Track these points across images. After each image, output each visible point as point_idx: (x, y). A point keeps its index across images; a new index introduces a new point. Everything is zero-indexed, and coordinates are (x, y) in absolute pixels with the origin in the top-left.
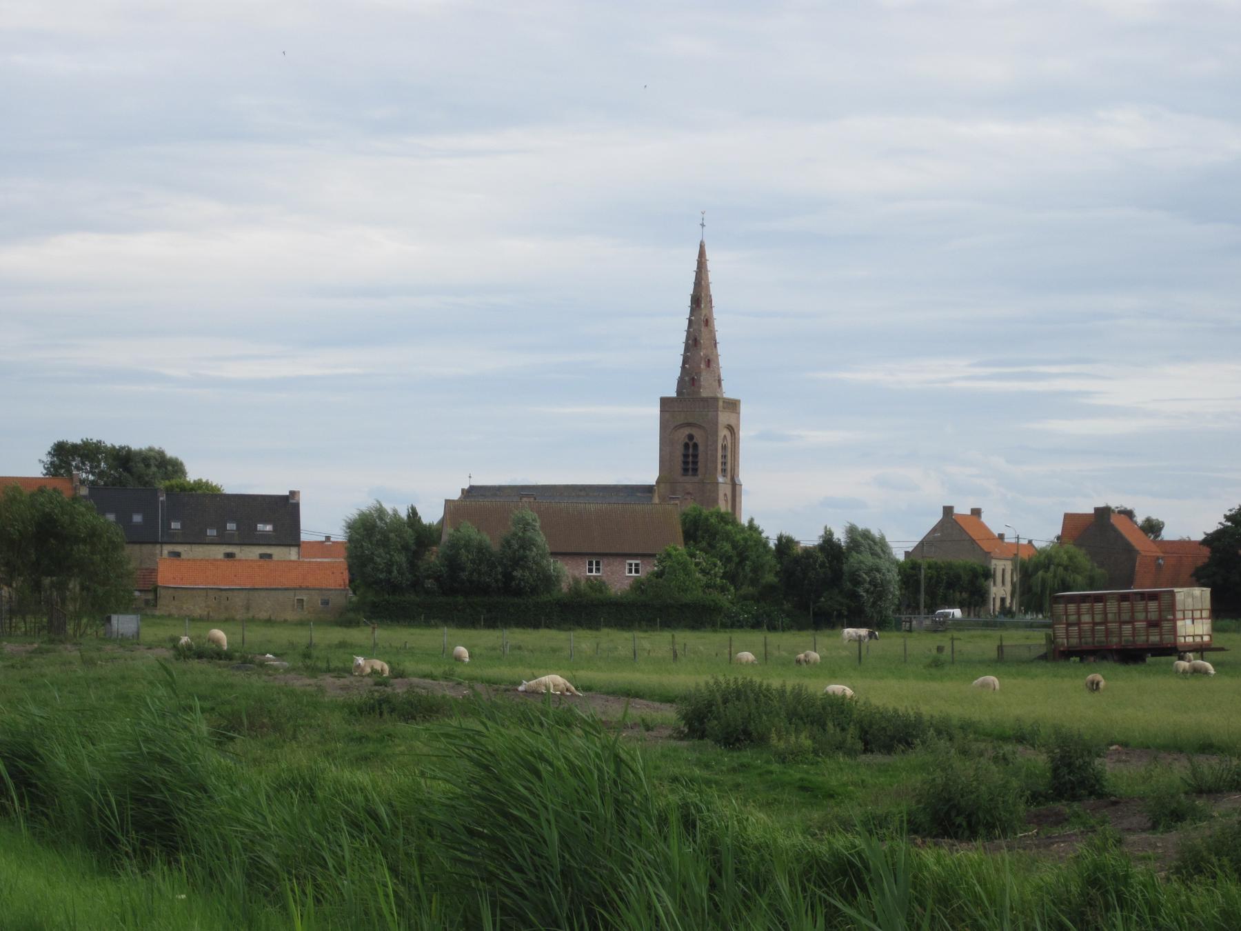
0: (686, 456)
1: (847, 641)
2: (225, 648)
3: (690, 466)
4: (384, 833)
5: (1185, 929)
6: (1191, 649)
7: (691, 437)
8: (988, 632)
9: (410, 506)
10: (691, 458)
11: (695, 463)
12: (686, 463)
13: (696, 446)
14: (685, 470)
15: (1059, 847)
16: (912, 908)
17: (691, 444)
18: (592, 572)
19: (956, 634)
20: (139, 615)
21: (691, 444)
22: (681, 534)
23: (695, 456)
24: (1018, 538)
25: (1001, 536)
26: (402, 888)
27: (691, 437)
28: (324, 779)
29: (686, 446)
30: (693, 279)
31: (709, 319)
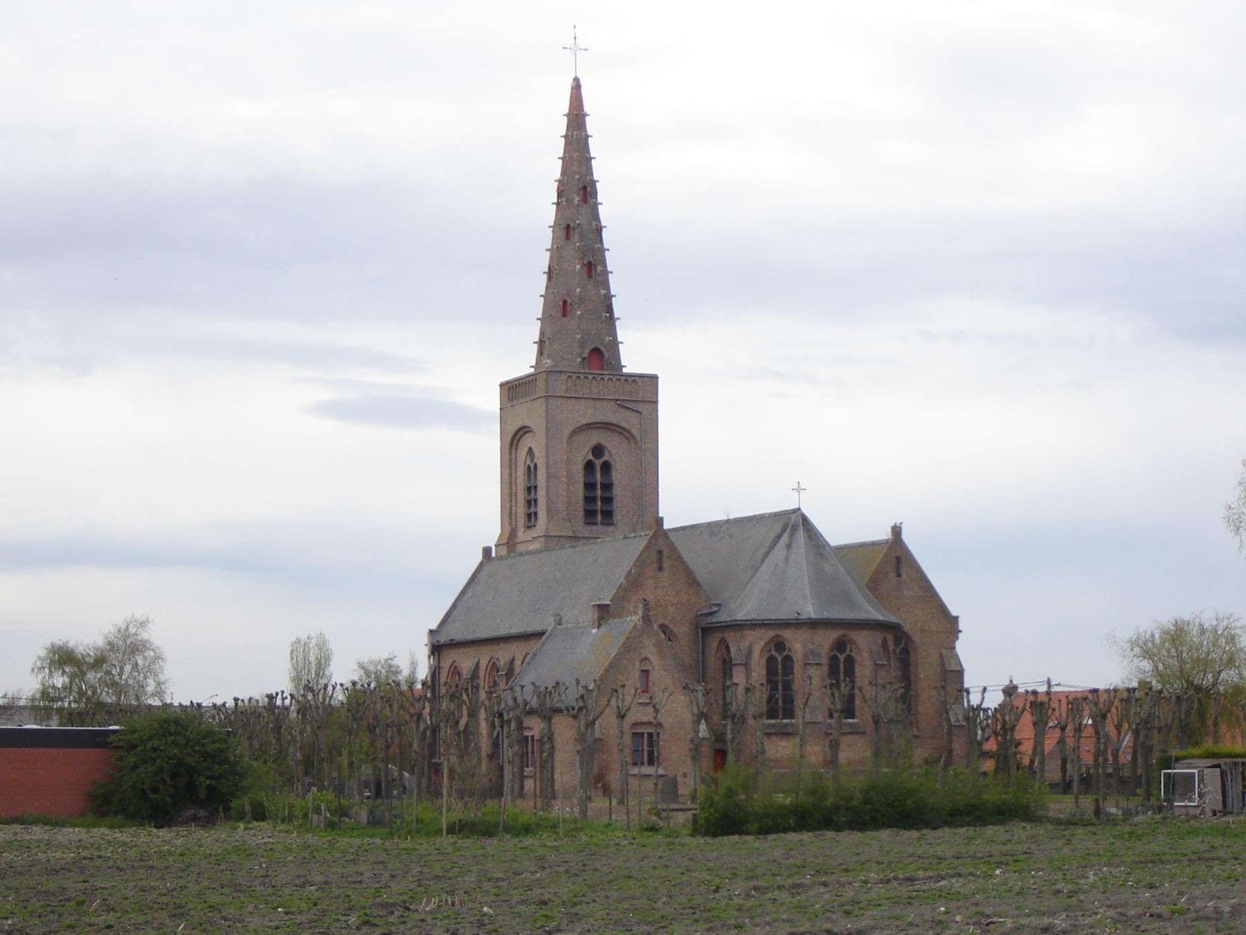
0: (589, 486)
1: (394, 679)
4: (160, 894)
7: (598, 450)
9: (356, 667)
10: (599, 503)
11: (608, 500)
12: (589, 499)
13: (606, 467)
14: (590, 515)
15: (923, 862)
17: (598, 463)
18: (649, 733)
19: (653, 720)
21: (598, 463)
23: (607, 487)
24: (1049, 682)
25: (224, 705)
27: (598, 450)
29: (589, 466)
31: (527, 520)
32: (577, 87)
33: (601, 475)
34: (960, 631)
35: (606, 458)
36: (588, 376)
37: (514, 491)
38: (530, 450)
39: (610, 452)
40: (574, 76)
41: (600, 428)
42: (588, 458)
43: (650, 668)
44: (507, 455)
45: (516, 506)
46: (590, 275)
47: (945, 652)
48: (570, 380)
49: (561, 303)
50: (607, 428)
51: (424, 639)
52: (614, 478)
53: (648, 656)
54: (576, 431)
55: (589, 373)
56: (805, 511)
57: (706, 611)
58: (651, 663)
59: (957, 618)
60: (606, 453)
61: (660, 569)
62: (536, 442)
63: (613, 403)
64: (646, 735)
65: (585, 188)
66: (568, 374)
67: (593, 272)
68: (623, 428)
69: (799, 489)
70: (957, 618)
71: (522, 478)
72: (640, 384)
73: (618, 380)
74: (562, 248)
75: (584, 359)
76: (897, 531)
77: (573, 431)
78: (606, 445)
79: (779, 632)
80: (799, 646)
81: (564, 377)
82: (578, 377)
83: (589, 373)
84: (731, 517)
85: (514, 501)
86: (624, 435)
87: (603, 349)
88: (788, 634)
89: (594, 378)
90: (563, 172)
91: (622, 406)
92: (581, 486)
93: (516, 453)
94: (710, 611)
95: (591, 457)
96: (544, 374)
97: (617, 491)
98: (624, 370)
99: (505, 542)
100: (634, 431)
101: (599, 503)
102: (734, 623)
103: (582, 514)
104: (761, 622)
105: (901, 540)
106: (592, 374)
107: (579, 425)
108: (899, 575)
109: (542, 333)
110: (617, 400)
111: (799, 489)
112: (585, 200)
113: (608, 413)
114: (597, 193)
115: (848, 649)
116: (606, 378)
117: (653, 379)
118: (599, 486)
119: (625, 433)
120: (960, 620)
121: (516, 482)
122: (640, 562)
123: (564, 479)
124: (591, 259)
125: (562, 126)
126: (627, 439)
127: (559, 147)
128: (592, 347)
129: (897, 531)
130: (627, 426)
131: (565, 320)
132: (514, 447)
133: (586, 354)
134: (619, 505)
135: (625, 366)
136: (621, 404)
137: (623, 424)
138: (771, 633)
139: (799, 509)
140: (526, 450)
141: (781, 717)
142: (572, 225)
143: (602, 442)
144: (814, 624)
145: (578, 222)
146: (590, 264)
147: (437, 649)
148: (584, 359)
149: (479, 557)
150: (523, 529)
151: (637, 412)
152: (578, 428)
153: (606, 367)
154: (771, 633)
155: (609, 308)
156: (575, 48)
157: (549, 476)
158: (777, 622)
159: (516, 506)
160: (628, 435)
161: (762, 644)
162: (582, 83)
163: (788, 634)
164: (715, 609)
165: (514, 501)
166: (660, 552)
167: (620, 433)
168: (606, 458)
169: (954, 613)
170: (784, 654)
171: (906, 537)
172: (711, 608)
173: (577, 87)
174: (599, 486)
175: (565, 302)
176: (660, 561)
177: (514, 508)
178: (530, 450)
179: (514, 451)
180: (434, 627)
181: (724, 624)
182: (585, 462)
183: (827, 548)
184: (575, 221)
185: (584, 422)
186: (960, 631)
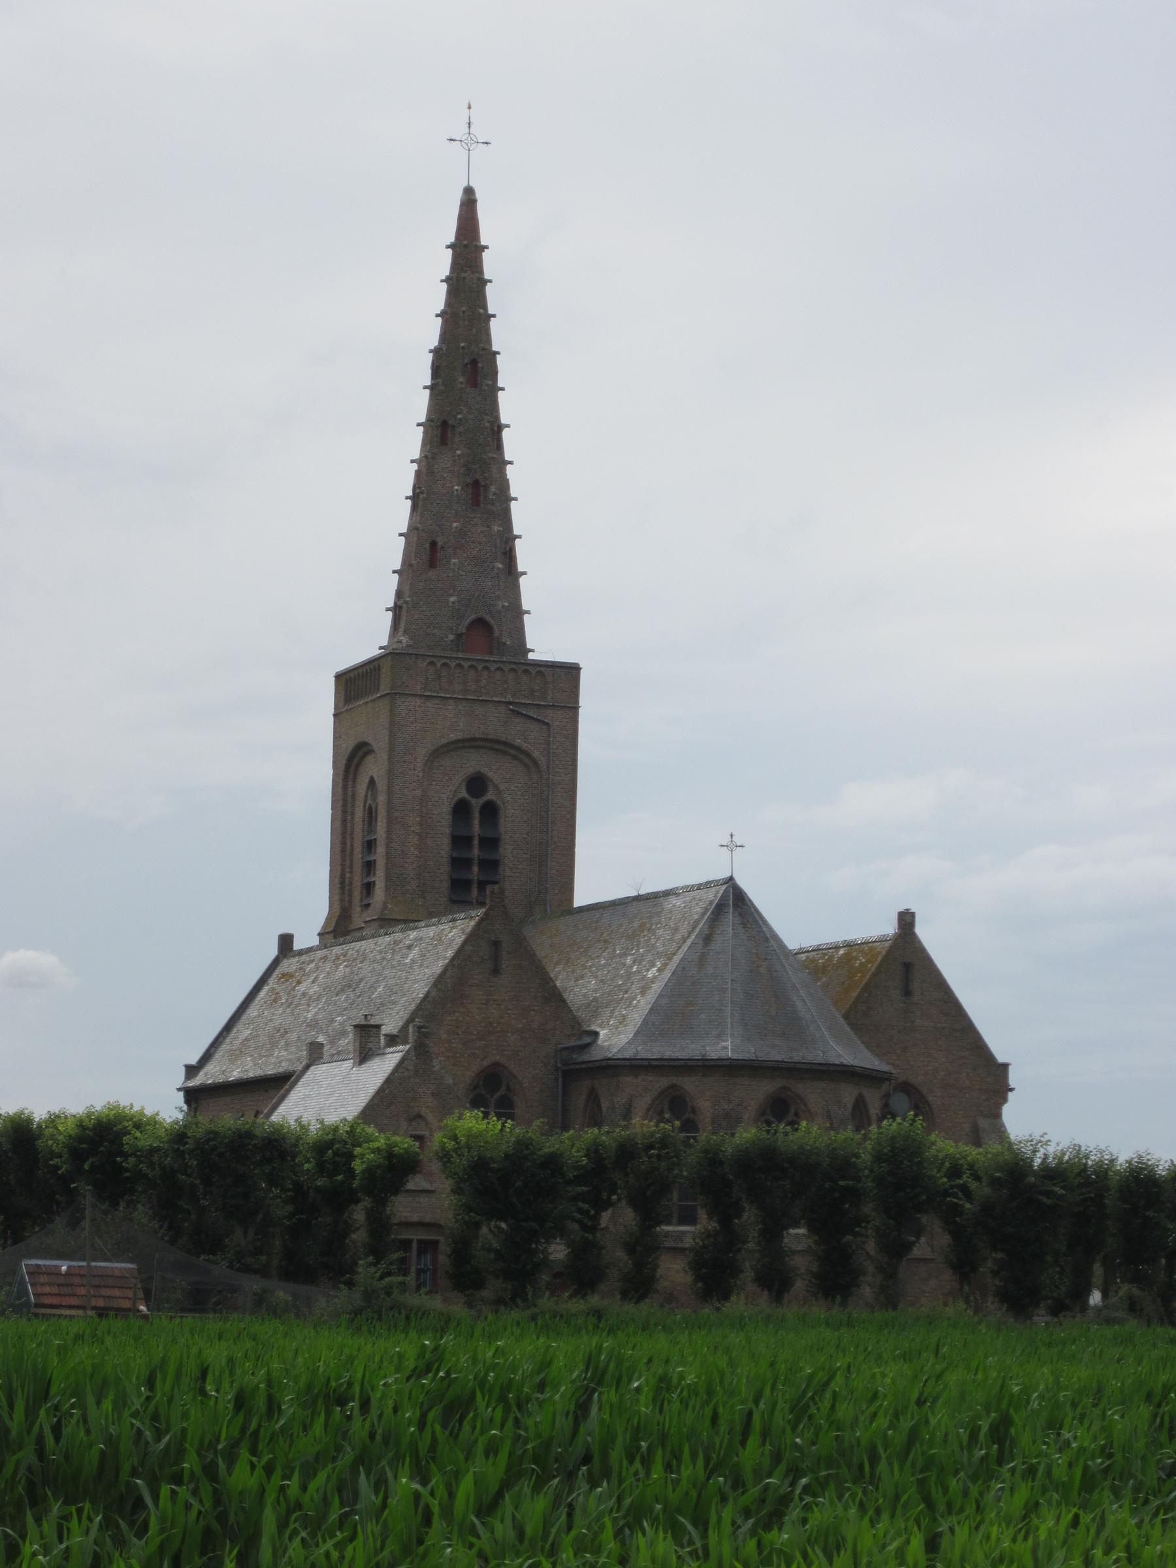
0: (460, 841)
2: (839, 1297)
3: (476, 852)
5: (846, 1550)
6: (220, 1040)
7: (477, 783)
8: (235, 1030)
10: (475, 869)
12: (460, 863)
13: (491, 811)
16: (423, 1030)
17: (476, 804)
20: (352, 1166)
21: (476, 804)
22: (377, 868)
23: (491, 843)
26: (345, 1386)
27: (477, 783)
28: (995, 1143)
29: (461, 810)
30: (431, 333)
31: (364, 892)
32: (469, 203)
33: (481, 823)
34: (1012, 1090)
35: (490, 796)
36: (463, 663)
37: (348, 847)
38: (372, 782)
39: (496, 787)
40: (465, 184)
41: (484, 747)
42: (460, 796)
43: (426, 1133)
44: (340, 789)
45: (351, 872)
46: (476, 501)
47: (983, 1123)
48: (432, 669)
49: (427, 546)
50: (470, 747)
51: (179, 1078)
52: (502, 829)
53: (422, 1113)
54: (438, 753)
55: (463, 659)
56: (742, 882)
57: (572, 1043)
58: (427, 1123)
59: (1005, 1067)
60: (491, 788)
61: (496, 971)
62: (375, 768)
63: (502, 708)
64: (415, 1245)
65: (474, 362)
66: (428, 660)
67: (481, 498)
68: (518, 749)
69: (732, 846)
70: (1005, 1067)
71: (360, 827)
72: (550, 679)
73: (512, 670)
74: (433, 458)
75: (459, 636)
76: (906, 920)
77: (436, 750)
78: (490, 774)
79: (675, 1080)
80: (707, 1104)
81: (423, 664)
82: (445, 665)
83: (450, 658)
84: (642, 893)
85: (348, 863)
86: (521, 761)
87: (492, 622)
88: (689, 1084)
89: (471, 666)
90: (445, 336)
91: (519, 713)
92: (446, 842)
93: (354, 786)
94: (579, 1043)
95: (464, 794)
96: (389, 658)
97: (507, 851)
98: (531, 656)
99: (331, 929)
100: (536, 754)
101: (475, 869)
102: (604, 1063)
103: (446, 884)
104: (646, 1063)
105: (914, 935)
106: (457, 658)
107: (444, 741)
108: (907, 993)
109: (399, 594)
110: (510, 703)
111: (732, 846)
112: (474, 382)
113: (493, 723)
114: (496, 373)
115: (792, 1111)
116: (493, 667)
117: (571, 672)
118: (476, 842)
119: (522, 757)
120: (1010, 1068)
121: (352, 834)
122: (461, 959)
123: (416, 828)
124: (478, 476)
125: (444, 262)
126: (526, 765)
127: (438, 297)
128: (473, 617)
129: (906, 920)
130: (525, 746)
131: (432, 574)
132: (351, 776)
133: (462, 629)
134: (508, 873)
135: (532, 651)
136: (516, 711)
137: (518, 742)
138: (664, 1082)
139: (731, 879)
140: (367, 780)
141: (675, 1221)
142: (451, 422)
143: (485, 770)
144: (731, 1069)
145: (459, 416)
146: (476, 484)
147: (193, 1096)
148: (459, 636)
149: (273, 952)
150: (359, 909)
151: (543, 722)
152: (444, 746)
153: (495, 651)
154: (664, 1082)
155: (509, 556)
156: (469, 141)
157: (390, 820)
158: (672, 1063)
159: (351, 872)
160: (526, 760)
161: (649, 1098)
162: (479, 195)
163: (689, 1084)
164: (587, 1040)
165: (348, 863)
166: (496, 944)
167: (515, 758)
168: (490, 796)
169: (1001, 1058)
170: (684, 1118)
171: (923, 932)
172: (580, 1038)
173: (469, 203)
174: (476, 842)
175: (433, 544)
176: (496, 958)
177: (348, 875)
178: (372, 782)
179: (350, 783)
180: (193, 1060)
181: (590, 1065)
182: (454, 802)
183: (772, 942)
184: (455, 416)
185: (453, 737)
186: (1012, 1090)
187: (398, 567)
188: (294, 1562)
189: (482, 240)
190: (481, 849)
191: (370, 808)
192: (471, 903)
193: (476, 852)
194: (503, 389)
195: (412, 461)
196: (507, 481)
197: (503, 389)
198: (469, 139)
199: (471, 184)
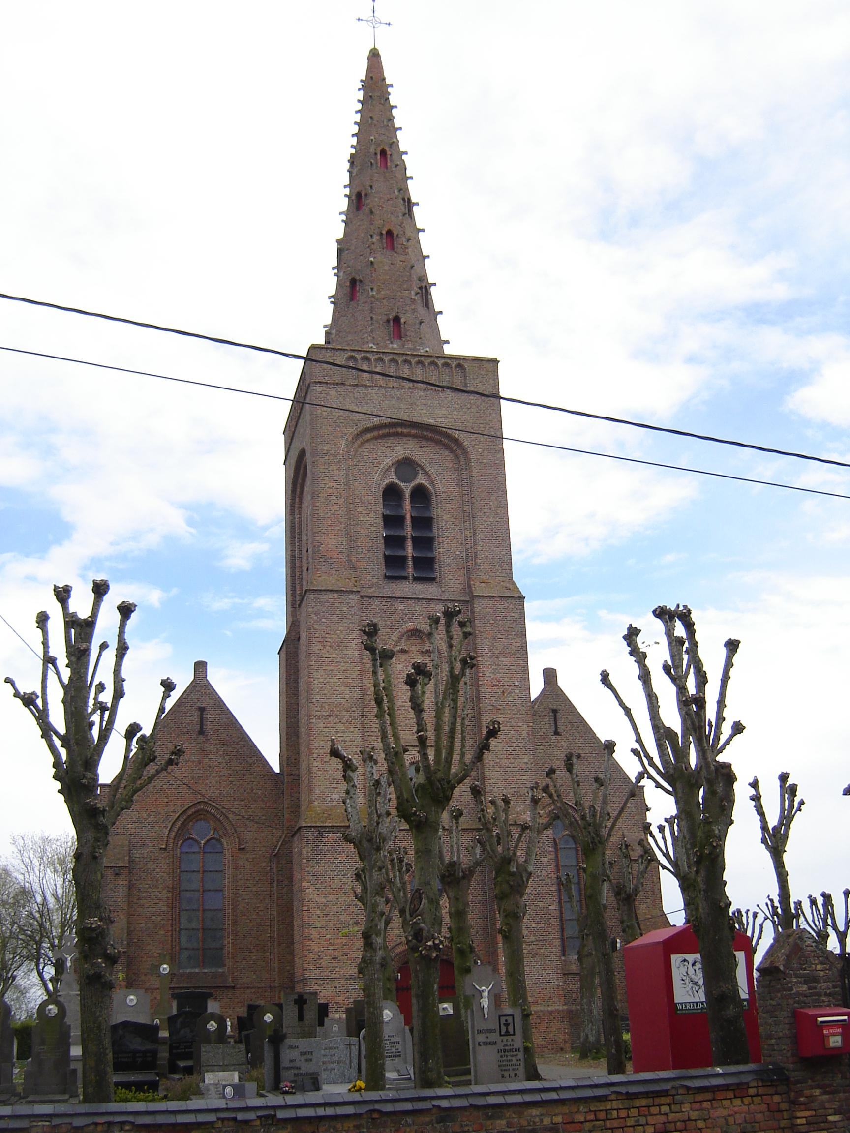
0: (392, 521)
3: (409, 550)
10: (409, 544)
13: (421, 495)
17: (407, 489)
21: (407, 489)
23: (424, 522)
27: (406, 466)
29: (391, 493)
32: (374, 56)
40: (373, 47)
98: (448, 350)
101: (409, 544)
156: (374, 21)
168: (420, 480)
173: (374, 56)
187: (426, 261)
188: (311, 805)
189: (446, 327)
190: (415, 547)
191: (302, 454)
192: (405, 578)
193: (409, 550)
194: (411, 178)
195: (341, 214)
196: (673, 683)
197: (411, 178)
198: (374, 20)
199: (376, 47)
